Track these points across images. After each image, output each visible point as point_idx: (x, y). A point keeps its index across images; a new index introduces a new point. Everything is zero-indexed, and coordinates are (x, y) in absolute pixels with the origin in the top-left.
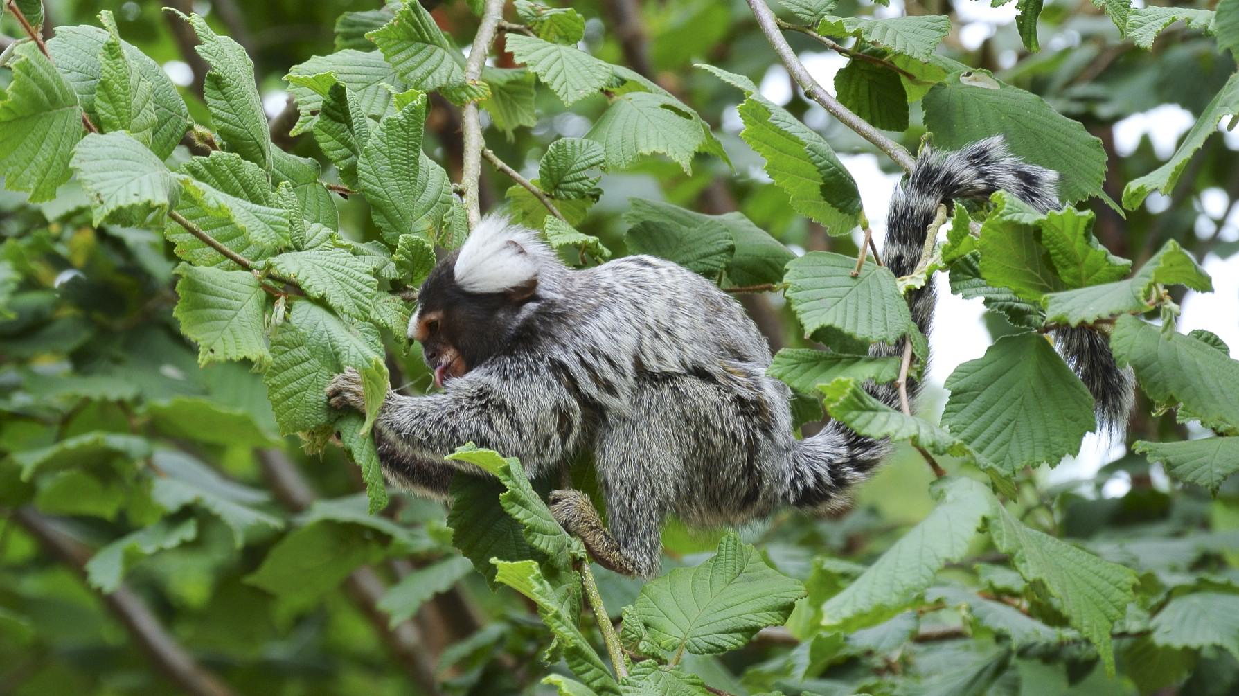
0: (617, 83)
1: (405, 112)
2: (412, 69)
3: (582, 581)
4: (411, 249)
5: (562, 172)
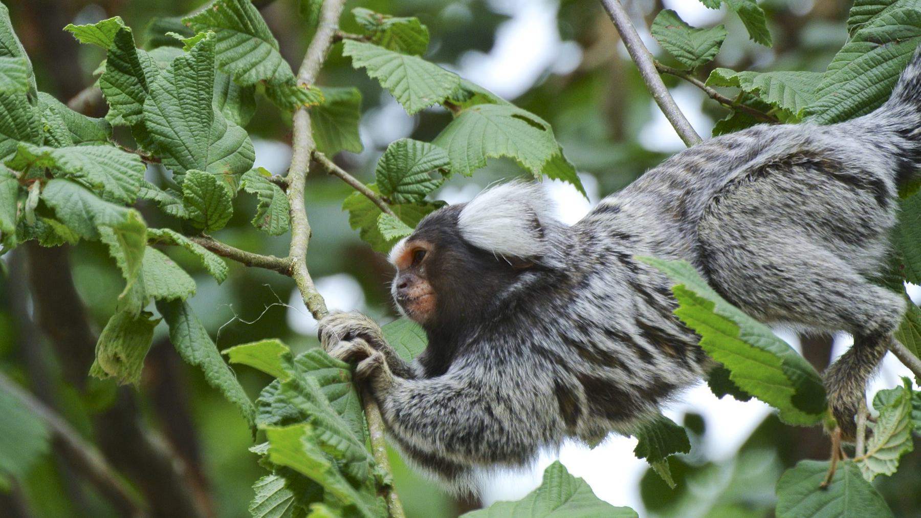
0: (464, 96)
1: (193, 51)
2: (233, 60)
3: (388, 509)
4: (200, 185)
5: (403, 172)
